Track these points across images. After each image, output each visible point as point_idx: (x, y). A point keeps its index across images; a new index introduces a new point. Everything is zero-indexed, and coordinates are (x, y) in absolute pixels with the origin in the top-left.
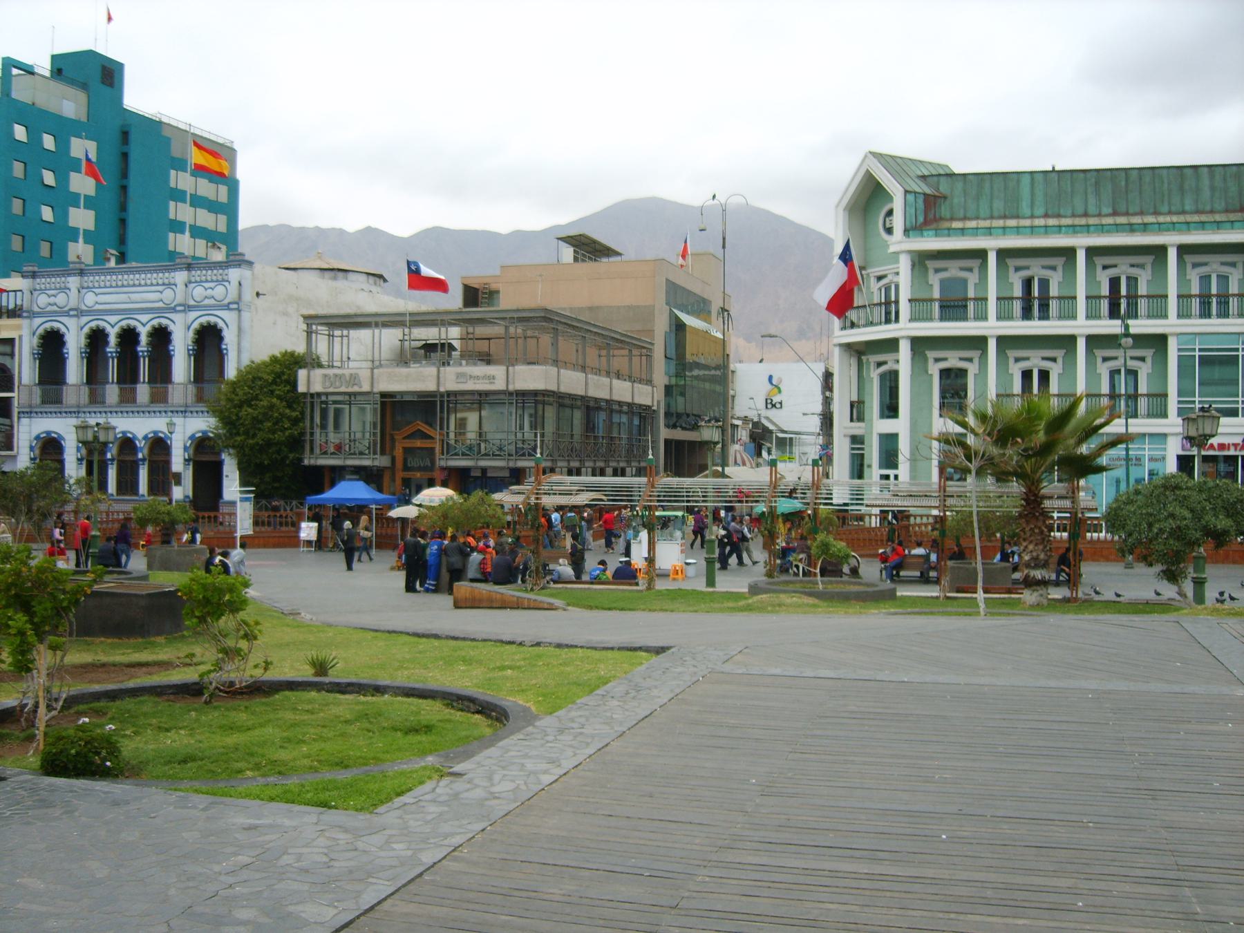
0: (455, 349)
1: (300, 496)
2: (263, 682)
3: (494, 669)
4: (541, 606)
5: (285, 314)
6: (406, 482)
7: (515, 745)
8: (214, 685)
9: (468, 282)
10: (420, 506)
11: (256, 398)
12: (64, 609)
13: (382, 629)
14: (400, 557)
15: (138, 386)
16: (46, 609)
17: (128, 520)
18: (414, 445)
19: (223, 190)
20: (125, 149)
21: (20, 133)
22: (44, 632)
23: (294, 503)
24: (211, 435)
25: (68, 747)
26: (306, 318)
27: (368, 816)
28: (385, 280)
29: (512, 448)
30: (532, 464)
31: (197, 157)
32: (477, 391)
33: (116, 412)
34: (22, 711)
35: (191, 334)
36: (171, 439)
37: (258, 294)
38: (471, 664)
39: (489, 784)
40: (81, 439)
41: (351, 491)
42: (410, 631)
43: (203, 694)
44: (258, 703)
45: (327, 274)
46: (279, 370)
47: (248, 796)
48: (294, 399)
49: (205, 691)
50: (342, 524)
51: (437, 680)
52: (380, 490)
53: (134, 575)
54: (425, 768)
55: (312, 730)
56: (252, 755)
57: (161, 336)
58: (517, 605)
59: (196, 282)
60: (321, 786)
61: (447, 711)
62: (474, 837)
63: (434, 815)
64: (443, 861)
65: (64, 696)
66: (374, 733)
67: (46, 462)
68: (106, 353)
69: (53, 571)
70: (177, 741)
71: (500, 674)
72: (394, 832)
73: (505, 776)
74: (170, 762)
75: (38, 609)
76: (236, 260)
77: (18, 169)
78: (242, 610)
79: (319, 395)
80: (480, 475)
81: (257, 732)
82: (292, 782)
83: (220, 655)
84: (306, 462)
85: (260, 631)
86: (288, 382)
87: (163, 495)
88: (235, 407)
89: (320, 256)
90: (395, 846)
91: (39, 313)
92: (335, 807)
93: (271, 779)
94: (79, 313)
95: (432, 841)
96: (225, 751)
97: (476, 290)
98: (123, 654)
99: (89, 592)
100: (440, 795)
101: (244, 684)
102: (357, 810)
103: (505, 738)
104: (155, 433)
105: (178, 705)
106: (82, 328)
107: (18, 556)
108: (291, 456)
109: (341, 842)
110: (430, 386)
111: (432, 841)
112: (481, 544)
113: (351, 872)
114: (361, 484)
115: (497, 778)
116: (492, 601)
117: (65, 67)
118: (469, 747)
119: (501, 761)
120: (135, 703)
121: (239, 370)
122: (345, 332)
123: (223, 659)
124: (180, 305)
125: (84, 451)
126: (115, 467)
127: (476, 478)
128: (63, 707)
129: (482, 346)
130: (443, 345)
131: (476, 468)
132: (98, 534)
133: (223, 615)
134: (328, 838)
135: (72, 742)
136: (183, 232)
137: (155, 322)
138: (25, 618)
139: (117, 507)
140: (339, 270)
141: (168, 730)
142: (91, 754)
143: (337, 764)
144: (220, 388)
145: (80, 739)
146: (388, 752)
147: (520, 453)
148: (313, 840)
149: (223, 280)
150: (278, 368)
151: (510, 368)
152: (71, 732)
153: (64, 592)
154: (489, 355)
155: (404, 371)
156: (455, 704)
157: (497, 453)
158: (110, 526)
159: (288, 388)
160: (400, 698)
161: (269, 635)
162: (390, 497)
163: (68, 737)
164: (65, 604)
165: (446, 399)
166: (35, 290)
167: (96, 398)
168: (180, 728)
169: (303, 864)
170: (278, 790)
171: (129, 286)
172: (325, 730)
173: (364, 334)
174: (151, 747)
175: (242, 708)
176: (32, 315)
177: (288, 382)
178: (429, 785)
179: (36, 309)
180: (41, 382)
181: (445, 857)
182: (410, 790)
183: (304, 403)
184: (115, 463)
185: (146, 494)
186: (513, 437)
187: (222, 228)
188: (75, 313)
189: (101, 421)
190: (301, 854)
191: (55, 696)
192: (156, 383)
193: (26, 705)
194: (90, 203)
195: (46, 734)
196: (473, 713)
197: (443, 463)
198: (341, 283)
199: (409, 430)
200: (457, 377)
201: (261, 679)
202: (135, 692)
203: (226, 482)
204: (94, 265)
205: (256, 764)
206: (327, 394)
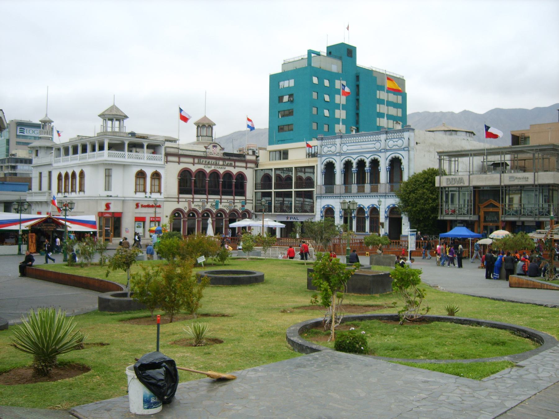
0: (508, 165)
1: (437, 234)
2: (426, 317)
3: (534, 317)
4: (553, 288)
5: (429, 151)
6: (485, 228)
7: (548, 355)
8: (404, 317)
9: (512, 134)
10: (492, 239)
11: (417, 189)
12: (343, 281)
13: (477, 295)
14: (483, 262)
15: (365, 185)
16: (335, 281)
17: (361, 243)
18: (489, 210)
19: (400, 98)
20: (358, 83)
21: (315, 80)
22: (334, 290)
23: (433, 236)
24: (397, 206)
25: (346, 339)
26: (438, 153)
27: (479, 382)
28: (474, 134)
29: (537, 211)
30: (549, 219)
31: (389, 84)
32: (519, 185)
33: (368, 196)
34: (325, 322)
35: (388, 162)
36: (379, 208)
37: (417, 143)
38: (522, 314)
39: (537, 373)
40: (343, 208)
41: (460, 231)
42: (490, 297)
43: (400, 321)
44: (424, 326)
45: (447, 133)
46: (427, 177)
47: (423, 367)
48: (434, 190)
49: (400, 319)
50: (458, 246)
51: (507, 321)
52: (473, 230)
53: (365, 267)
54: (504, 362)
55: (449, 340)
56: (423, 349)
57: (375, 163)
58: (541, 287)
59: (390, 139)
60: (456, 366)
61: (512, 335)
62: (531, 397)
63: (511, 385)
64: (516, 407)
65: (342, 317)
66: (478, 343)
67: (328, 218)
68: (352, 171)
69: (339, 264)
70: (389, 340)
71: (537, 320)
72: (491, 391)
73: (544, 369)
74: (386, 350)
75: (332, 280)
76: (407, 128)
77: (315, 95)
78: (418, 284)
79: (445, 188)
80: (521, 224)
81: (424, 339)
82: (443, 363)
83: (407, 304)
84: (439, 218)
85: (425, 294)
86: (431, 182)
87: (375, 232)
88: (407, 194)
89: (444, 125)
90: (492, 397)
91: (324, 155)
92: (463, 376)
93: (433, 361)
94: (341, 154)
95: (510, 397)
96: (411, 346)
97: (518, 137)
98: (362, 301)
99: (353, 274)
100: (512, 376)
101: (418, 317)
102: (473, 378)
103: (543, 351)
104: (373, 205)
105: (389, 325)
106: (342, 161)
107: (325, 257)
108: (432, 216)
109: (467, 393)
110: (497, 183)
111: (510, 397)
112: (522, 257)
113: (472, 407)
114: (465, 228)
115: (540, 370)
116: (528, 285)
117: (332, 51)
118: (525, 354)
119: (542, 362)
120: (371, 323)
121: (409, 177)
122: (456, 159)
123: (409, 306)
124: (383, 149)
125: (343, 213)
126: (355, 219)
127: (519, 226)
128: (341, 322)
129: (522, 163)
130: (503, 163)
131: (519, 221)
132: (350, 248)
133: (409, 286)
134: (461, 390)
135: (347, 338)
136: (383, 117)
137: (372, 157)
138: (328, 284)
139: (358, 237)
140: (453, 131)
141: (385, 335)
142: (355, 343)
143: (461, 357)
144: (401, 185)
145: (351, 336)
146: (485, 353)
147: (541, 214)
148: (454, 390)
149: (401, 138)
150: (426, 176)
151: (536, 174)
152: (347, 333)
153: (343, 273)
154: (525, 167)
155: (484, 176)
156: (516, 333)
157: (529, 214)
158: (354, 245)
159: (431, 185)
160: (489, 328)
161: (429, 296)
162: (477, 234)
163: (346, 335)
164: (343, 278)
165: (504, 189)
166: (323, 145)
167: (348, 191)
168: (391, 335)
169: (450, 401)
170: (436, 366)
171: (361, 142)
172: (455, 341)
173: (465, 160)
174: (379, 342)
175: (417, 328)
176: (322, 156)
177: (431, 182)
178: (507, 370)
179: (323, 153)
180: (325, 184)
181: (517, 405)
182: (498, 371)
183: (438, 191)
184: (356, 218)
185: (369, 232)
186: (538, 207)
187: (400, 114)
188: (339, 154)
189: (351, 200)
190: (449, 396)
191: (338, 317)
192: (360, 184)
193: (326, 320)
194: (344, 107)
195: (335, 333)
196: (525, 338)
197: (503, 219)
198: (454, 137)
199: (487, 203)
200: (510, 178)
201: (425, 315)
202: (370, 318)
203: (403, 227)
204: (346, 133)
205: (425, 353)
206: (448, 187)
